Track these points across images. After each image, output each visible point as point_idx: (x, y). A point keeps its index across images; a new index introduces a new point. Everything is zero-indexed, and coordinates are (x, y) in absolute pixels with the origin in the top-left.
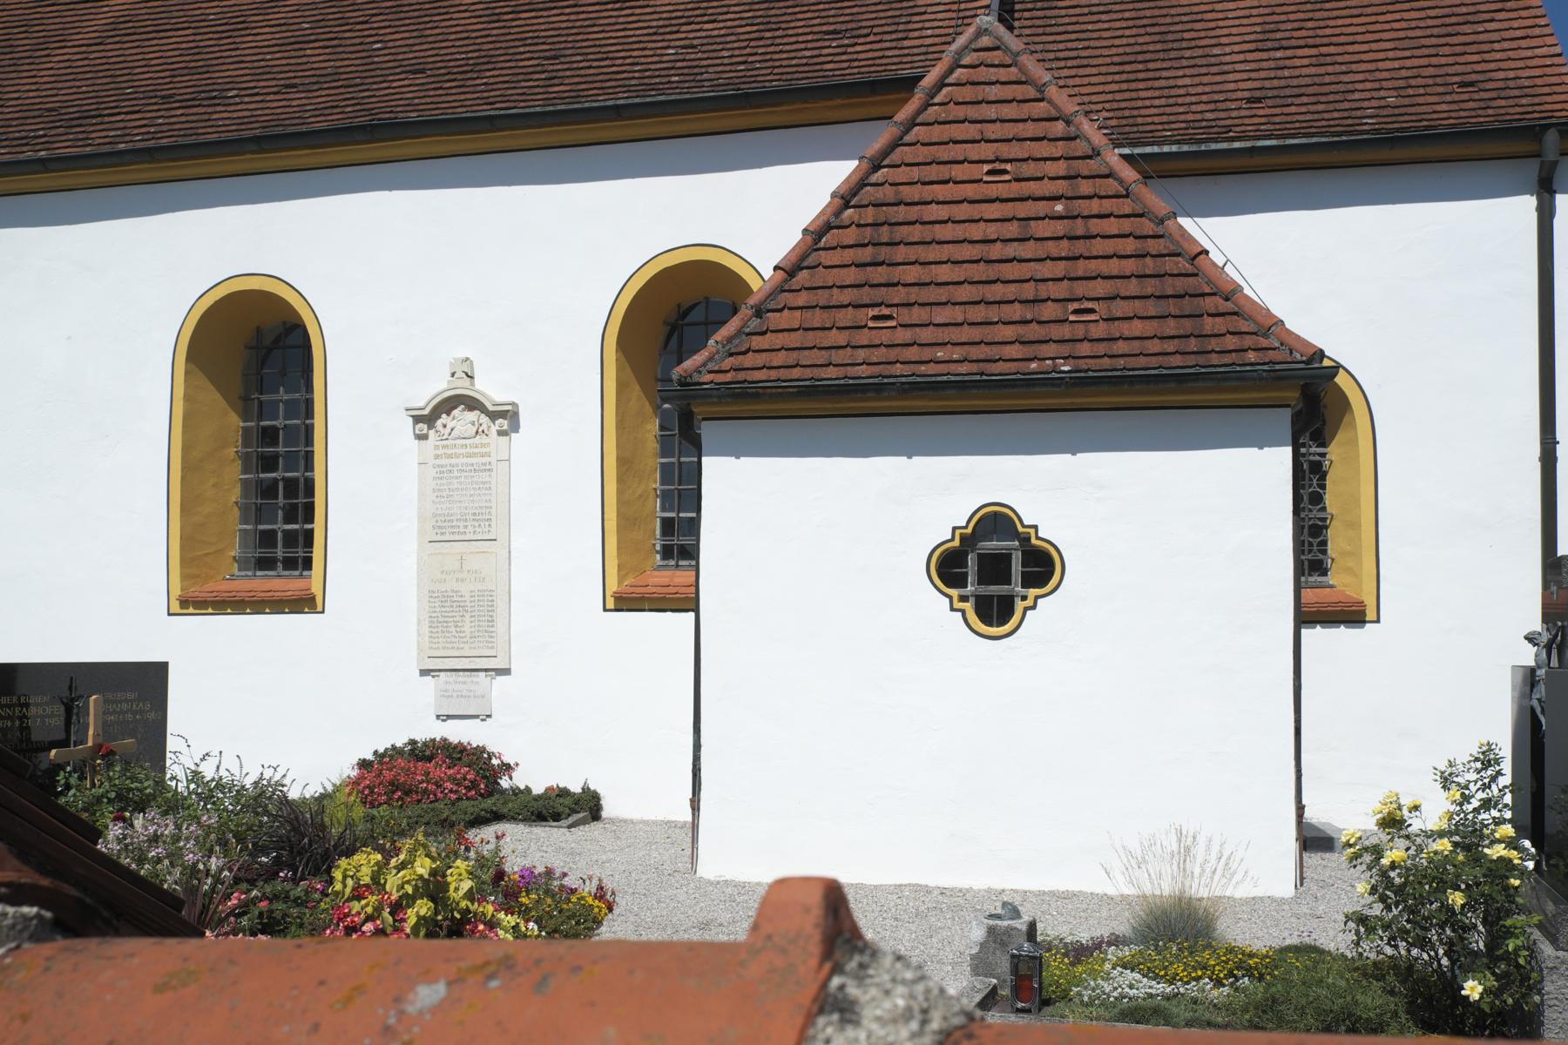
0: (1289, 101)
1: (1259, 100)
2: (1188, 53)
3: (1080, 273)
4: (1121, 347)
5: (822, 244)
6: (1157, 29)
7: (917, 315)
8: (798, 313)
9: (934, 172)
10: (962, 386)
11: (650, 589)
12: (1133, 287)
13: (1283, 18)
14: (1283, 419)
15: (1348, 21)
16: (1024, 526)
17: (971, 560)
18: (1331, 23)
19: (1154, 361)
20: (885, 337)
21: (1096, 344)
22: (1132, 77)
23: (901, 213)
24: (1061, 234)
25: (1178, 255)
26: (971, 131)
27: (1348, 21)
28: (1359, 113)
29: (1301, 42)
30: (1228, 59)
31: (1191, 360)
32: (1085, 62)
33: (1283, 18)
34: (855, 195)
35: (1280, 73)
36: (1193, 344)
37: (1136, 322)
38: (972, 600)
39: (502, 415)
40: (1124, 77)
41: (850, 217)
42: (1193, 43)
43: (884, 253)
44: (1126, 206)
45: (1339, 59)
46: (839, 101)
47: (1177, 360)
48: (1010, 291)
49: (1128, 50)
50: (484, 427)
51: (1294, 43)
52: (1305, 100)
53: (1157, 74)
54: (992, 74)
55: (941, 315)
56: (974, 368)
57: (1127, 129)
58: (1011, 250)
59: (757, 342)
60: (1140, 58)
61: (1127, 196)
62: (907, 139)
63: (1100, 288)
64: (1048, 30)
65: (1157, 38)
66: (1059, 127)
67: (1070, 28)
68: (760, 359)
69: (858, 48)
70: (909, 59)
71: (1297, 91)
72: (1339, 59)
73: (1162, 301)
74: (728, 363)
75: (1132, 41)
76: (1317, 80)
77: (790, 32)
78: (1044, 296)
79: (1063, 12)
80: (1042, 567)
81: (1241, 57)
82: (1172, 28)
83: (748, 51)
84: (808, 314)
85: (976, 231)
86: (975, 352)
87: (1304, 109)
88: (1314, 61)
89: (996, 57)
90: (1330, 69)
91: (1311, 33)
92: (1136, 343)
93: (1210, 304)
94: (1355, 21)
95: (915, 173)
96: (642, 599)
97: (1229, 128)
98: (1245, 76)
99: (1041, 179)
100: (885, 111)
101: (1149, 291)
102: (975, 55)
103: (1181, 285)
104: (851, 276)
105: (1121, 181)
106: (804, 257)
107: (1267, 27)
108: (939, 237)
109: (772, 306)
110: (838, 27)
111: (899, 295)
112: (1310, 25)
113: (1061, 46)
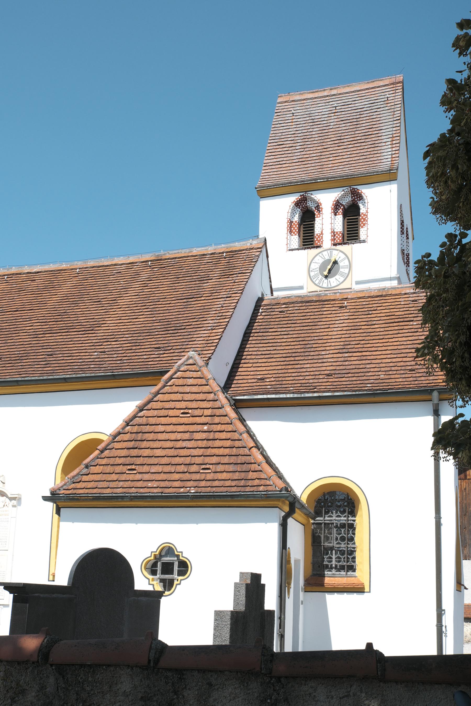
3: (208, 454)
4: (216, 483)
5: (116, 440)
7: (146, 469)
8: (102, 467)
10: (153, 498)
12: (226, 460)
16: (177, 552)
17: (159, 564)
19: (226, 489)
20: (131, 477)
21: (207, 482)
23: (148, 428)
24: (204, 438)
26: (179, 397)
31: (239, 489)
34: (131, 421)
36: (242, 483)
37: (225, 473)
39: (14, 499)
41: (128, 430)
44: (230, 428)
50: (7, 504)
55: (154, 469)
58: (184, 444)
59: (85, 478)
61: (231, 424)
62: (155, 399)
63: (215, 460)
65: (302, 346)
66: (211, 396)
73: (236, 465)
74: (73, 486)
76: (357, 367)
78: (193, 463)
84: (105, 467)
85: (173, 436)
88: (359, 358)
93: (253, 467)
95: (155, 413)
101: (231, 462)
103: (243, 459)
104: (124, 453)
107: (346, 343)
109: (93, 464)
111: (139, 461)
112: (362, 342)
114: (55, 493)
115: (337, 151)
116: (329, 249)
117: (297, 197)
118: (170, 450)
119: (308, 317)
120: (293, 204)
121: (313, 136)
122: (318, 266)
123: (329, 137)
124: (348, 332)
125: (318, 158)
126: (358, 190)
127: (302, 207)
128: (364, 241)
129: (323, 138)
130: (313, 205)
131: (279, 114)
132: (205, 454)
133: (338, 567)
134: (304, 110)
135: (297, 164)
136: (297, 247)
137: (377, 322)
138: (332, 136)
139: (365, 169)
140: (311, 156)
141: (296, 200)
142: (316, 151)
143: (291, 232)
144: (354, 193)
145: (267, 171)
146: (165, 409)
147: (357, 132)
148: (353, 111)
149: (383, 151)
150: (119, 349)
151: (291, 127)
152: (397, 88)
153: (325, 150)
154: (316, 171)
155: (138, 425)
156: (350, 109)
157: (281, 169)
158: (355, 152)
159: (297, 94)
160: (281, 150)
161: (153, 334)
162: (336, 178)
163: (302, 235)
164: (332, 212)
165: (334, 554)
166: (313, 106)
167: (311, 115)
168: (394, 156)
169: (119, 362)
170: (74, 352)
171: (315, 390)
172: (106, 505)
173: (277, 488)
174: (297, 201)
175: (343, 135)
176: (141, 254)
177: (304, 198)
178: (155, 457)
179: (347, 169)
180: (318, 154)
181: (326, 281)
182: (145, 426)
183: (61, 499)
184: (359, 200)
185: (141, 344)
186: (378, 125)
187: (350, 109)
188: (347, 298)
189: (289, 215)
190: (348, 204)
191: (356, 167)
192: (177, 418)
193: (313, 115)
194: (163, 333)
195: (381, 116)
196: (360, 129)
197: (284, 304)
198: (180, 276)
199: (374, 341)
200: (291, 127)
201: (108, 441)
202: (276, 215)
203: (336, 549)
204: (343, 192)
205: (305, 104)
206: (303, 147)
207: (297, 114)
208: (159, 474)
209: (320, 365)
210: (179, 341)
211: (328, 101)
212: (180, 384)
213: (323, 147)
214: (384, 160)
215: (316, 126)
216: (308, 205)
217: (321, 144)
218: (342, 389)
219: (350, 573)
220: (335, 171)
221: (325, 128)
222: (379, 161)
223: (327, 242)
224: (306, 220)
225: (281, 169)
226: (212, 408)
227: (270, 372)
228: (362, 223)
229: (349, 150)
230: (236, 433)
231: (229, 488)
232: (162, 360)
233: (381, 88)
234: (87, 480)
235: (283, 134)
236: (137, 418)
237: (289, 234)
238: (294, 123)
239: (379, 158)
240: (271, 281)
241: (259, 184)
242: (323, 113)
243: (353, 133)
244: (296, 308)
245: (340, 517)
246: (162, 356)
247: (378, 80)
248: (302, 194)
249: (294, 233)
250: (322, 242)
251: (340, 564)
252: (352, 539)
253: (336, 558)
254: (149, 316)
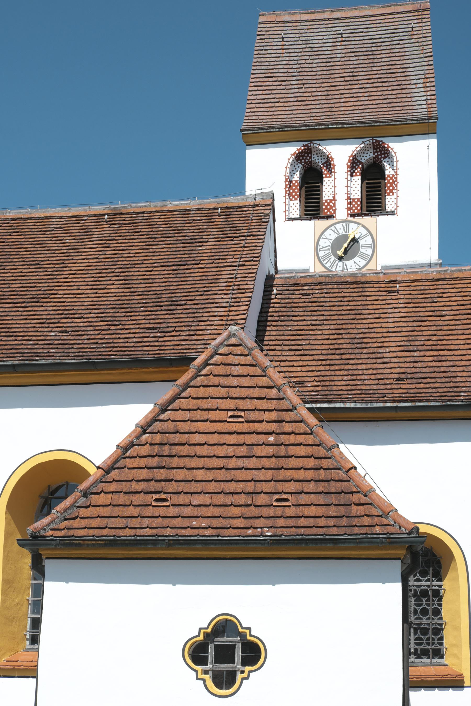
0: (420, 381)
1: (403, 379)
2: (365, 351)
3: (281, 478)
4: (302, 522)
5: (127, 455)
6: (348, 336)
7: (183, 499)
8: (109, 496)
9: (198, 415)
10: (206, 543)
11: (19, 663)
12: (311, 487)
13: (420, 333)
14: (396, 567)
15: (456, 337)
17: (211, 648)
18: (447, 338)
19: (321, 531)
20: (162, 512)
21: (288, 520)
22: (333, 362)
23: (177, 438)
24: (271, 454)
25: (339, 469)
26: (222, 392)
27: (456, 337)
28: (458, 389)
29: (429, 348)
30: (387, 355)
31: (342, 531)
32: (306, 352)
33: (420, 333)
34: (150, 426)
35: (416, 365)
36: (344, 522)
38: (210, 673)
40: (328, 362)
41: (146, 439)
42: (368, 345)
43: (165, 461)
44: (310, 439)
45: (450, 358)
46: (151, 369)
47: (334, 531)
48: (239, 487)
49: (331, 347)
51: (425, 348)
52: (429, 380)
53: (347, 362)
54: (236, 360)
55: (197, 500)
56: (214, 532)
57: (327, 393)
58: (242, 463)
59: (83, 512)
60: (338, 352)
61: (311, 434)
62: (184, 395)
63: (293, 487)
64: (286, 333)
65: (348, 341)
66: (274, 393)
67: (299, 333)
68: (84, 523)
69: (166, 339)
70: (195, 347)
71: (424, 375)
72: (450, 358)
74: (65, 524)
75: (334, 342)
76: (436, 369)
77: (126, 327)
78: (259, 490)
79: (296, 323)
80: (253, 653)
81: (395, 355)
82: (357, 336)
83: (100, 336)
84: (116, 496)
85: (221, 451)
86: (216, 523)
87: (428, 386)
88: (435, 358)
89: (239, 350)
90: (444, 364)
91: (435, 343)
92: (312, 520)
93: (356, 498)
94: (460, 337)
95: (187, 415)
96: (14, 669)
97: (385, 395)
98: (396, 365)
99: (262, 421)
100: (172, 376)
101: (321, 489)
102: (227, 348)
103: (339, 486)
104: (144, 474)
105: (308, 425)
106: (116, 462)
107: (411, 338)
108: (199, 453)
109: (94, 490)
110: (155, 326)
111: (171, 487)
112: (434, 338)
113: (293, 343)
114: (37, 534)
115: (350, 91)
116: (345, 221)
117: (299, 148)
118: (219, 471)
119: (346, 303)
120: (293, 157)
121: (315, 69)
122: (329, 243)
123: (337, 71)
124: (410, 324)
125: (324, 97)
126: (383, 143)
127: (305, 162)
128: (393, 213)
129: (328, 72)
130: (320, 160)
131: (263, 37)
132: (277, 479)
133: (419, 652)
134: (297, 35)
135: (296, 104)
136: (298, 216)
137: (448, 313)
138: (341, 71)
139: (392, 116)
140: (313, 94)
141: (297, 152)
142: (321, 89)
143: (290, 195)
144: (377, 148)
145: (252, 110)
146: (201, 410)
147: (374, 69)
148: (366, 42)
149: (415, 95)
150: (89, 329)
151: (281, 55)
152: (424, 16)
153: (333, 88)
154: (323, 114)
155: (161, 433)
156: (361, 38)
157: (273, 109)
158: (375, 94)
159: (285, 14)
160: (271, 84)
161: (138, 310)
162: (355, 124)
163: (303, 201)
164: (348, 171)
165: (412, 634)
166: (309, 31)
167: (308, 42)
168: (429, 102)
169: (94, 346)
170: (17, 330)
171: (386, 398)
172: (123, 554)
173: (402, 528)
174: (299, 153)
175: (355, 70)
176: (89, 205)
177: (308, 149)
178: (196, 481)
179: (368, 114)
180: (323, 93)
181: (340, 264)
182: (174, 435)
183: (50, 544)
184: (385, 158)
185: (123, 323)
186: (404, 62)
187: (361, 38)
188: (396, 281)
189: (288, 171)
190: (367, 163)
191: (380, 113)
192: (222, 423)
193: (311, 42)
194: (152, 309)
195: (406, 50)
196: (378, 64)
197: (306, 284)
198: (156, 236)
199: (451, 337)
200: (281, 55)
201: (116, 456)
202: (268, 170)
203: (415, 626)
204: (362, 145)
205: (298, 28)
206: (301, 82)
207: (289, 39)
208: (207, 508)
209: (381, 366)
210: (182, 320)
211: (330, 26)
212: (221, 374)
213: (329, 85)
214: (417, 107)
215: (317, 57)
216: (313, 159)
217: (327, 80)
218: (426, 398)
219: (436, 660)
220: (350, 116)
221: (330, 60)
222: (411, 108)
223: (341, 211)
225: (273, 109)
226: (277, 410)
227: (309, 374)
228: (389, 189)
229: (367, 90)
230: (320, 447)
231: (325, 529)
232: (163, 346)
233: (402, 15)
234: (89, 515)
235: (272, 63)
236: (158, 422)
237: (287, 197)
238: (284, 51)
239: (410, 104)
240: (276, 256)
242: (324, 41)
243: (370, 69)
244: (325, 291)
245: (420, 581)
246: (161, 339)
247: (397, 5)
248: (305, 143)
249: (294, 197)
250: (335, 211)
251: (422, 647)
252: (437, 612)
253: (415, 640)
254: (122, 286)
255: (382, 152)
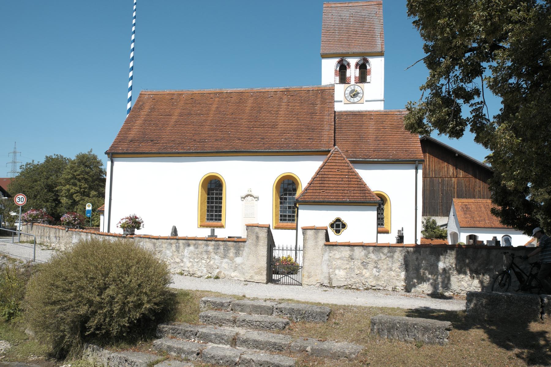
4: (355, 197)
12: (357, 189)
14: (376, 208)
20: (324, 194)
26: (334, 164)
36: (364, 197)
48: (340, 188)
58: (340, 182)
63: (352, 189)
89: (338, 153)
95: (327, 170)
111: (325, 188)
122: (349, 92)
202: (329, 68)
223: (353, 81)
224: (343, 68)
241: (321, 52)
252: (382, 214)
255: (366, 61)
